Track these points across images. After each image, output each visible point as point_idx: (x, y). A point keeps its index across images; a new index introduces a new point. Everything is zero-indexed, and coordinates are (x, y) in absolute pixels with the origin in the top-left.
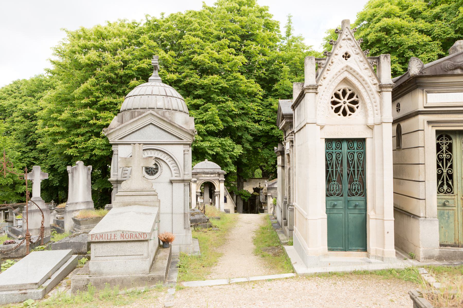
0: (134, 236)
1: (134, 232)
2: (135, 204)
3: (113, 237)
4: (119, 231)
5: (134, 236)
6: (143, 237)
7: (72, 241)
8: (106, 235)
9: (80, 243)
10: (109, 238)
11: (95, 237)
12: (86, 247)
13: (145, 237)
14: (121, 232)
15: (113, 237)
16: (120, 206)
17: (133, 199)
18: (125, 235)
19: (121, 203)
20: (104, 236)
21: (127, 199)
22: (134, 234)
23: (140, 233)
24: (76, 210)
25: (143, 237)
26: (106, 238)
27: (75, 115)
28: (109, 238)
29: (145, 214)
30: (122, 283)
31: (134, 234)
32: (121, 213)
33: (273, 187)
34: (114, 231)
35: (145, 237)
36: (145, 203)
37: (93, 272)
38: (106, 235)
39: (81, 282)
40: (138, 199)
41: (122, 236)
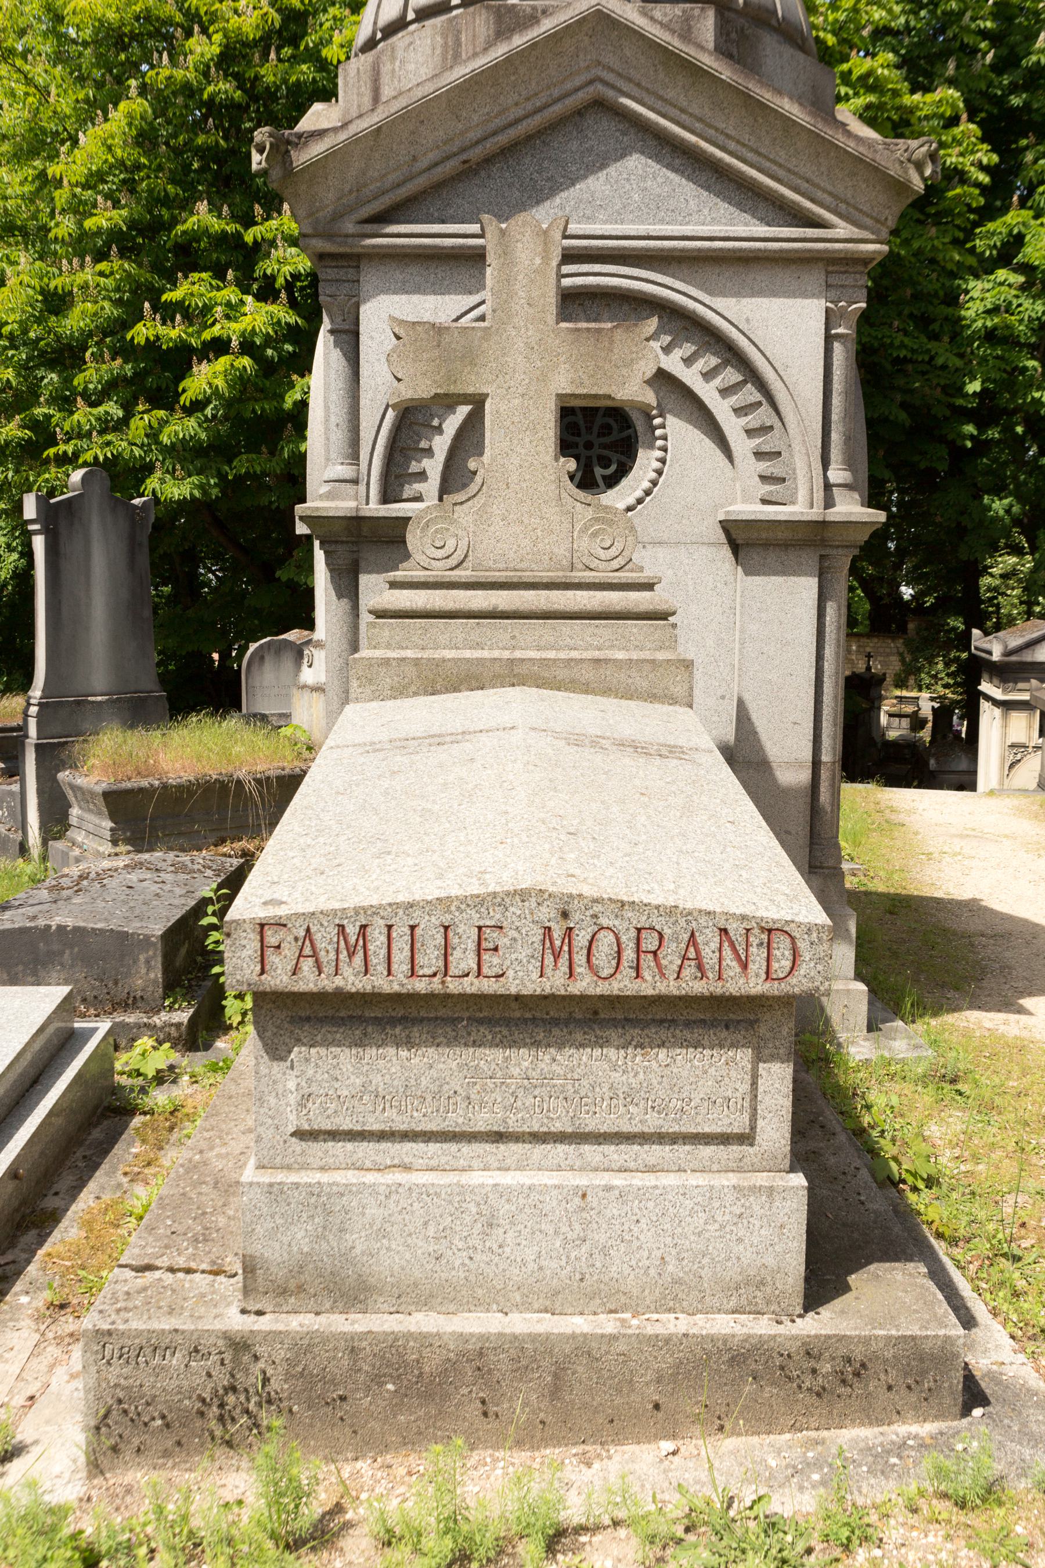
0: (671, 958)
1: (671, 911)
2: (513, 674)
3: (464, 959)
4: (523, 895)
5: (671, 958)
6: (757, 964)
7: (70, 922)
8: (401, 932)
9: (123, 936)
10: (430, 959)
11: (290, 951)
12: (158, 963)
13: (782, 964)
14: (547, 913)
15: (464, 959)
16: (400, 692)
17: (494, 644)
18: (581, 939)
19: (410, 671)
20: (377, 939)
21: (452, 643)
22: (675, 932)
23: (735, 929)
24: (424, 171)
25: (757, 964)
26: (400, 965)
27: (56, 303)
28: (430, 959)
29: (636, 748)
30: (555, 1391)
31: (675, 932)
32: (438, 740)
33: (1028, 657)
34: (479, 902)
35: (782, 964)
36: (588, 674)
37: (279, 1274)
38: (401, 932)
39: (176, 1361)
40: (531, 643)
41: (556, 944)
